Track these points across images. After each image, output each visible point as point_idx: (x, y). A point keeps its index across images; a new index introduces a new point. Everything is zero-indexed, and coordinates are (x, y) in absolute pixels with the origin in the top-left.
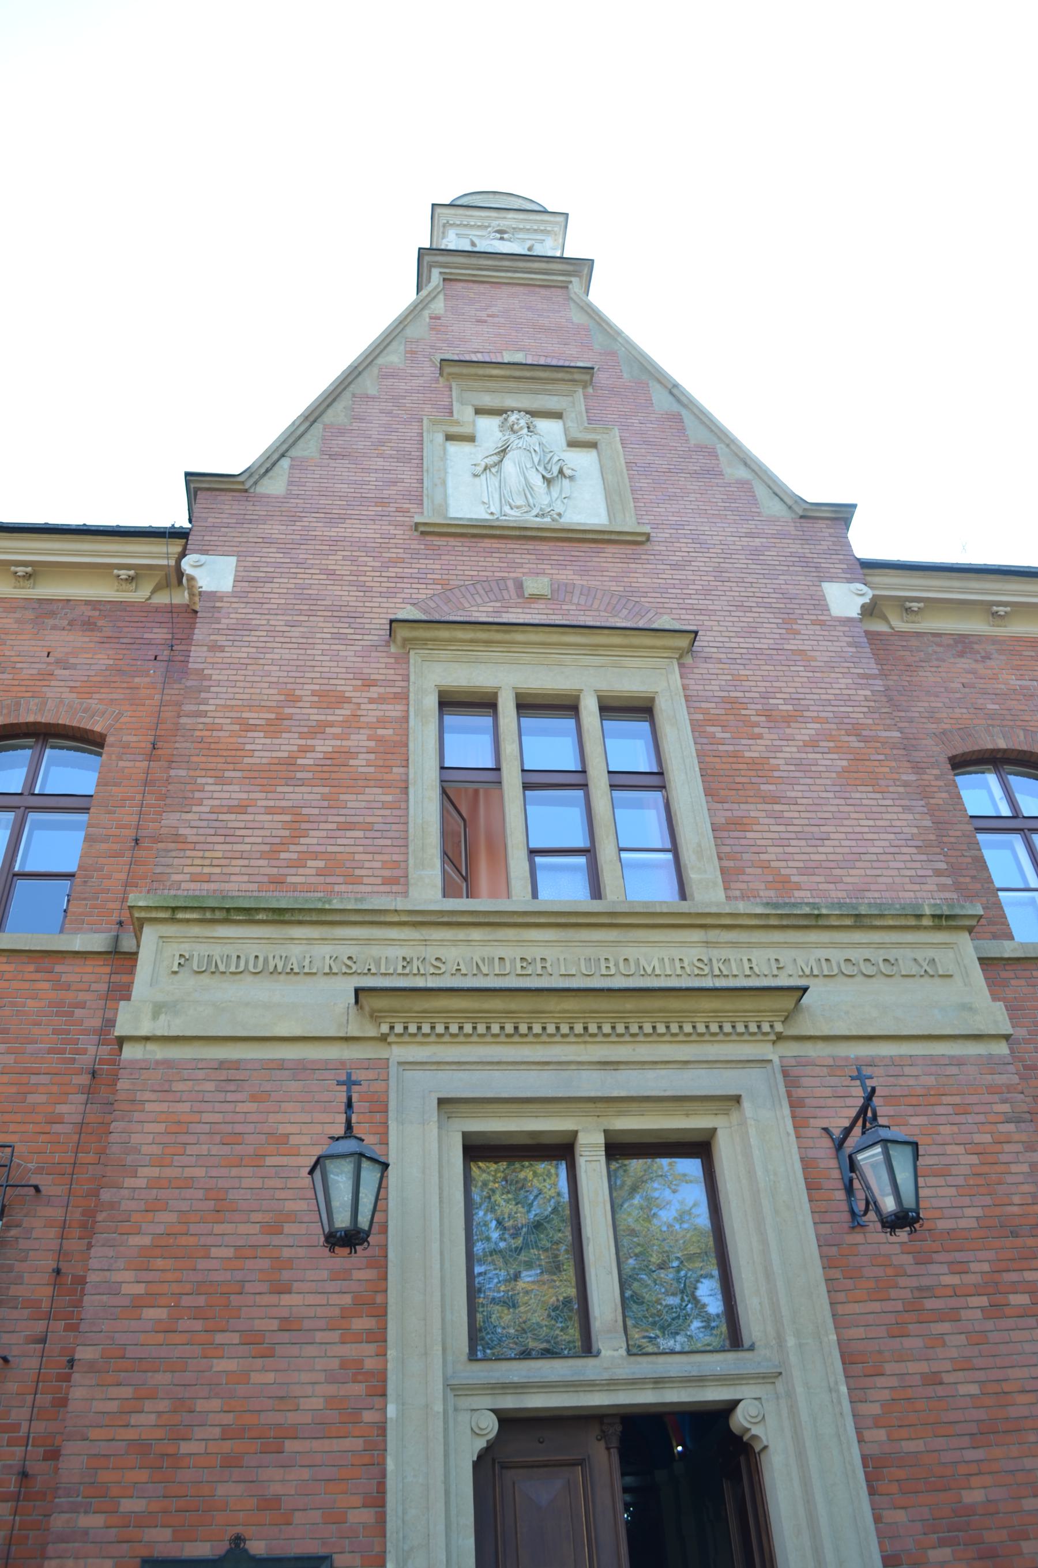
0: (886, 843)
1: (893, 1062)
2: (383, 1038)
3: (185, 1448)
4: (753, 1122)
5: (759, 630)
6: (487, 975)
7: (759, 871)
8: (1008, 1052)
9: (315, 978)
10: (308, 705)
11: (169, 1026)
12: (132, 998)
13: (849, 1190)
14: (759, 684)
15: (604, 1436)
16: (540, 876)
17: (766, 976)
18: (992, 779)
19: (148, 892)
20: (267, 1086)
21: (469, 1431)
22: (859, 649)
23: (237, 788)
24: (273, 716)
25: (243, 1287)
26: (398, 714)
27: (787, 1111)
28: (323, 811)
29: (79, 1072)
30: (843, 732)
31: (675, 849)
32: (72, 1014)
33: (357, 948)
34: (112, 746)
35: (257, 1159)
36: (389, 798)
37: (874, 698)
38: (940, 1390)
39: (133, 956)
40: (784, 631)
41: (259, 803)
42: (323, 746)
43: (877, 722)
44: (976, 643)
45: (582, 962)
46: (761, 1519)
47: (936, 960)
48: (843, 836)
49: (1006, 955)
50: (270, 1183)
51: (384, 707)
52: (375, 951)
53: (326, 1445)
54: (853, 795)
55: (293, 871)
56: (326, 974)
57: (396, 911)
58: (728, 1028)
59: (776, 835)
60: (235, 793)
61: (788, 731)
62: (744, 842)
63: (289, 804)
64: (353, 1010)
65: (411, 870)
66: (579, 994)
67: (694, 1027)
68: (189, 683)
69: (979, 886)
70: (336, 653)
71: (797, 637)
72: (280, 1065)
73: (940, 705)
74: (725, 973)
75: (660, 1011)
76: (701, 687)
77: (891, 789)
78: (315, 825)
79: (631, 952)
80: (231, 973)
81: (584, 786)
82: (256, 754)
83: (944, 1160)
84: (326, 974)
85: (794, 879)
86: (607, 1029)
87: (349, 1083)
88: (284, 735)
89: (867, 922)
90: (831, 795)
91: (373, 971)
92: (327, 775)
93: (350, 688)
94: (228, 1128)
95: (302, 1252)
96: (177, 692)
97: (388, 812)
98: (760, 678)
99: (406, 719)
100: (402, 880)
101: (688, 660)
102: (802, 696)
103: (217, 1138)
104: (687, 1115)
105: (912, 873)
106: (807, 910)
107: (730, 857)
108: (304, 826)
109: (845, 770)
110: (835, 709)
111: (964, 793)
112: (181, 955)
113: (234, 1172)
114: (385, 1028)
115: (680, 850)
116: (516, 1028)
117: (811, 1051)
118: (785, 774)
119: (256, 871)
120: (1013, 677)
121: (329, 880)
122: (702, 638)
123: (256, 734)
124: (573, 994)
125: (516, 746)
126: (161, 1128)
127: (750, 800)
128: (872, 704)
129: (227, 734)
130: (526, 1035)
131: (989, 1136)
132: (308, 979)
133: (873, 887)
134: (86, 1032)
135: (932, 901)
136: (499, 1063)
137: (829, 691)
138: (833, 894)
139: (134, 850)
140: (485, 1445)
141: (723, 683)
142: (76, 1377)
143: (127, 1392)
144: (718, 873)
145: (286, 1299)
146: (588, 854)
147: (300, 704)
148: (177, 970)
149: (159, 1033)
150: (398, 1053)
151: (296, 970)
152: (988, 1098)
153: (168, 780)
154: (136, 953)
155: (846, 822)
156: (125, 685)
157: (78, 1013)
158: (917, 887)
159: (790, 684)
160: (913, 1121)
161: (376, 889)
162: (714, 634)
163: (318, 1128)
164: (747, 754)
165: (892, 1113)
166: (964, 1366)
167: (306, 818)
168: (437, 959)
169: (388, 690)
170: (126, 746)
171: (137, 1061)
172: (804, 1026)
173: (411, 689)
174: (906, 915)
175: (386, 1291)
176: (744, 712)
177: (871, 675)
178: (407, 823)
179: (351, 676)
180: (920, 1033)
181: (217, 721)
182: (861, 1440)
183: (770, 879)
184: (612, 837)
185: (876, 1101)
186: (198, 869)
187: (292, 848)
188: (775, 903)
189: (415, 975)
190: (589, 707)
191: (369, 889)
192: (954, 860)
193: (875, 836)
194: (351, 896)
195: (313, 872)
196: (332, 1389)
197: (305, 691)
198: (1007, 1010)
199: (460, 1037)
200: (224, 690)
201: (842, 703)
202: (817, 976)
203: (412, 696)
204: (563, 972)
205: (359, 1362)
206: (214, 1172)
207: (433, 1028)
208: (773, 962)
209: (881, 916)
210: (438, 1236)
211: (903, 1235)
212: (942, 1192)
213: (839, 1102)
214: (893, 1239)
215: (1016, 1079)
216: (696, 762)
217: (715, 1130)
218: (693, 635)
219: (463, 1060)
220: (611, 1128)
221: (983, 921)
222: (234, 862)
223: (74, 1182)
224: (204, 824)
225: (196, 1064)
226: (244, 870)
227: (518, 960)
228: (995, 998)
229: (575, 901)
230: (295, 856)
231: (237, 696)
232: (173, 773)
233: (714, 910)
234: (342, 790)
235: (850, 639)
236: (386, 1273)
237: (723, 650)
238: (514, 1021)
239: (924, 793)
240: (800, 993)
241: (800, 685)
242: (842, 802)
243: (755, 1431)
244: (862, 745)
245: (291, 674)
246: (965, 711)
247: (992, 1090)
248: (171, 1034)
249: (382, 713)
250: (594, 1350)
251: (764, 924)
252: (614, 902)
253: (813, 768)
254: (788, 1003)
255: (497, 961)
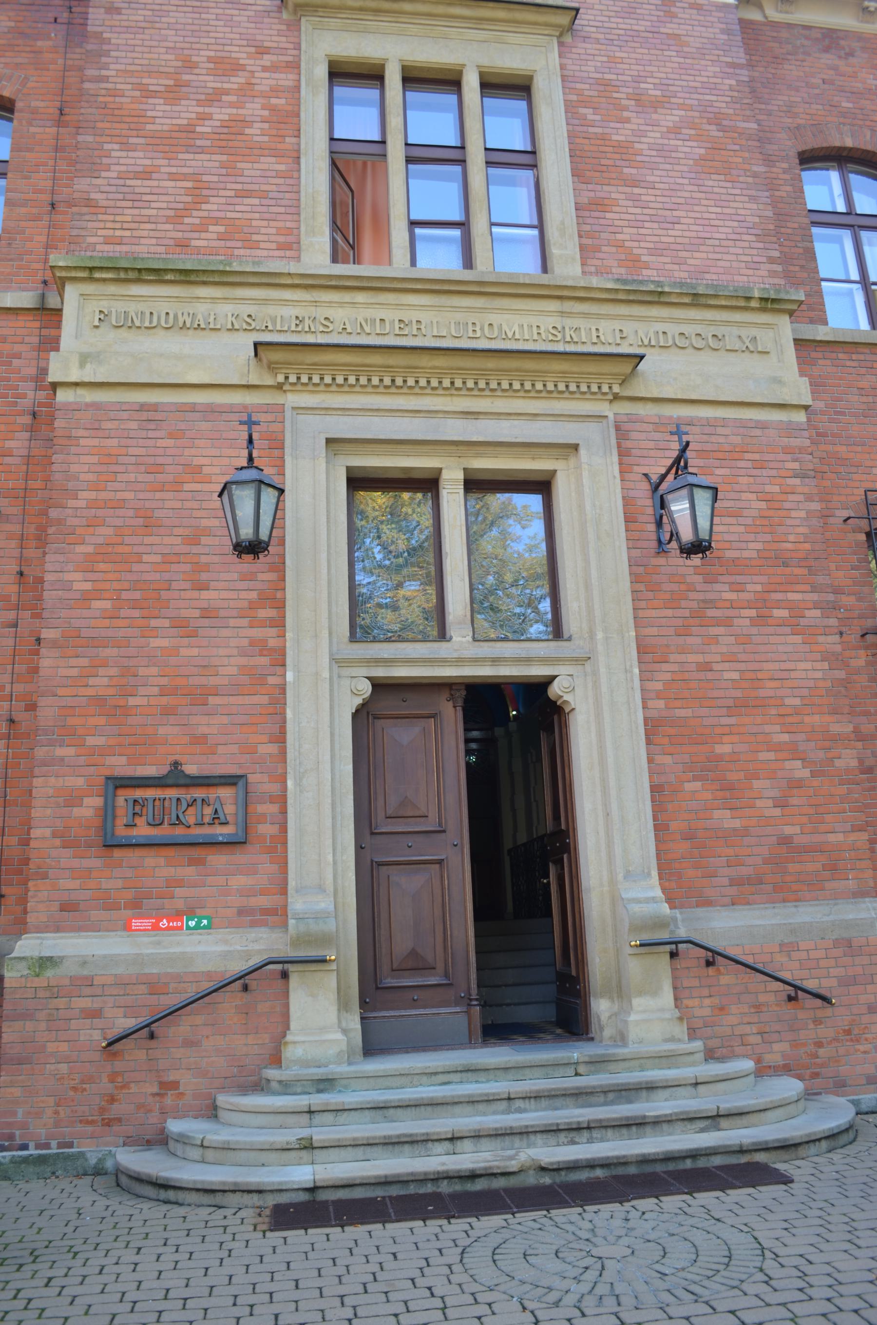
0: (730, 230)
1: (709, 423)
2: (279, 387)
3: (132, 701)
4: (586, 467)
5: (638, 11)
6: (369, 334)
7: (614, 249)
8: (805, 420)
9: (219, 333)
10: (204, 72)
11: (95, 373)
12: (61, 349)
13: (659, 524)
14: (633, 67)
15: (452, 698)
16: (420, 247)
17: (610, 344)
18: (834, 176)
19: (67, 253)
20: (182, 425)
21: (349, 692)
22: (731, 37)
23: (141, 154)
24: (171, 82)
25: (170, 584)
26: (290, 83)
27: (615, 458)
28: (222, 179)
29: (22, 413)
30: (705, 121)
31: (540, 226)
32: (10, 364)
33: (256, 307)
34: (21, 111)
35: (177, 485)
36: (282, 167)
37: (738, 88)
38: (710, 676)
39: (59, 312)
40: (662, 14)
41: (163, 170)
42: (220, 114)
43: (737, 112)
44: (843, 39)
45: (453, 325)
46: (566, 758)
47: (758, 338)
48: (692, 221)
49: (819, 338)
50: (188, 505)
51: (277, 76)
52: (271, 310)
53: (240, 700)
54: (707, 183)
55: (196, 235)
56: (228, 330)
57: (289, 274)
58: (573, 387)
59: (632, 217)
60: (140, 160)
61: (654, 116)
62: (602, 221)
63: (191, 170)
64: (253, 361)
65: (303, 237)
66: (448, 352)
67: (545, 385)
68: (89, 47)
69: (805, 275)
70: (229, 18)
71: (675, 20)
72: (192, 408)
73: (799, 99)
74: (575, 340)
75: (517, 370)
76: (578, 68)
77: (741, 179)
78: (215, 192)
79: (495, 318)
80: (146, 328)
81: (462, 162)
82: (158, 121)
83: (739, 504)
84: (228, 330)
85: (644, 258)
86: (470, 384)
87: (250, 423)
88: (183, 102)
89: (703, 301)
90: (686, 181)
91: (270, 328)
92: (223, 143)
93: (244, 56)
94: (151, 460)
95: (216, 559)
96: (78, 56)
97: (281, 181)
98: (634, 61)
99: (298, 88)
100: (295, 245)
101: (568, 39)
102: (671, 82)
103: (142, 468)
104: (533, 459)
105: (749, 259)
106: (652, 287)
107: (590, 235)
108: (205, 192)
109: (703, 158)
110: (701, 97)
111: (806, 188)
112: (101, 312)
113: (158, 495)
114: (281, 378)
115: (545, 227)
116: (393, 381)
117: (642, 410)
118: (647, 159)
119: (162, 234)
120: (871, 76)
121: (229, 244)
122: (583, 16)
123: (157, 101)
124: (443, 352)
125: (401, 119)
126: (95, 459)
127: (612, 182)
128: (736, 94)
129: (128, 100)
130: (402, 387)
131: (778, 487)
132: (213, 334)
133: (712, 270)
134: (24, 379)
135: (762, 286)
136: (378, 410)
137: (697, 78)
138: (676, 274)
139: (51, 214)
140: (361, 702)
141: (599, 64)
142: (43, 651)
143: (84, 662)
144: (578, 250)
145: (205, 594)
146: (463, 227)
147: (196, 71)
148: (97, 324)
149: (87, 380)
150: (292, 399)
151: (203, 326)
152: (782, 456)
153: (77, 147)
154: (61, 310)
155: (696, 208)
156: (28, 49)
157: (16, 362)
158: (751, 272)
159: (661, 69)
160: (718, 472)
161: (271, 253)
162: (595, 12)
163: (226, 461)
164: (614, 137)
165: (702, 465)
166: (729, 658)
167: (206, 185)
168: (326, 319)
169: (281, 58)
170: (35, 111)
171: (70, 403)
172: (638, 389)
173: (303, 58)
174: (737, 297)
175: (284, 589)
176: (615, 95)
177: (739, 64)
178: (298, 192)
179: (245, 43)
180: (734, 400)
181: (119, 86)
182: (645, 707)
183: (623, 257)
184: (485, 212)
185: (688, 454)
186: (110, 233)
187: (195, 213)
188: (624, 280)
189: (306, 332)
190: (471, 83)
191: (265, 253)
192: (787, 250)
193: (721, 223)
194: (250, 259)
195: (215, 236)
196: (243, 661)
197: (201, 57)
198: (811, 385)
199: (345, 387)
200: (123, 54)
201: (708, 91)
202: (654, 346)
203: (303, 65)
204: (435, 334)
205: (264, 641)
206: (141, 496)
207: (322, 379)
208: (617, 332)
209: (716, 296)
210: (326, 549)
211: (696, 559)
212: (732, 529)
213: (660, 453)
214: (688, 562)
215: (807, 442)
216: (566, 142)
217: (555, 471)
218: (574, 13)
219: (347, 406)
220: (470, 467)
221: (803, 307)
222: (143, 226)
223: (27, 504)
224: (113, 189)
225: (121, 407)
226: (152, 234)
227: (397, 322)
228: (802, 373)
229: (449, 270)
230: (197, 221)
231: (136, 61)
232: (80, 138)
233: (570, 283)
234: (240, 158)
235: (724, 26)
236: (284, 576)
237: (602, 30)
238: (392, 374)
239: (771, 185)
240: (637, 360)
241: (670, 70)
242: (695, 188)
243: (566, 697)
244: (721, 134)
245: (187, 39)
246: (820, 107)
247: (787, 450)
248: (97, 381)
249: (274, 82)
250: (448, 636)
251: (612, 298)
252: (483, 272)
253: (673, 155)
254: (626, 368)
255: (378, 321)
